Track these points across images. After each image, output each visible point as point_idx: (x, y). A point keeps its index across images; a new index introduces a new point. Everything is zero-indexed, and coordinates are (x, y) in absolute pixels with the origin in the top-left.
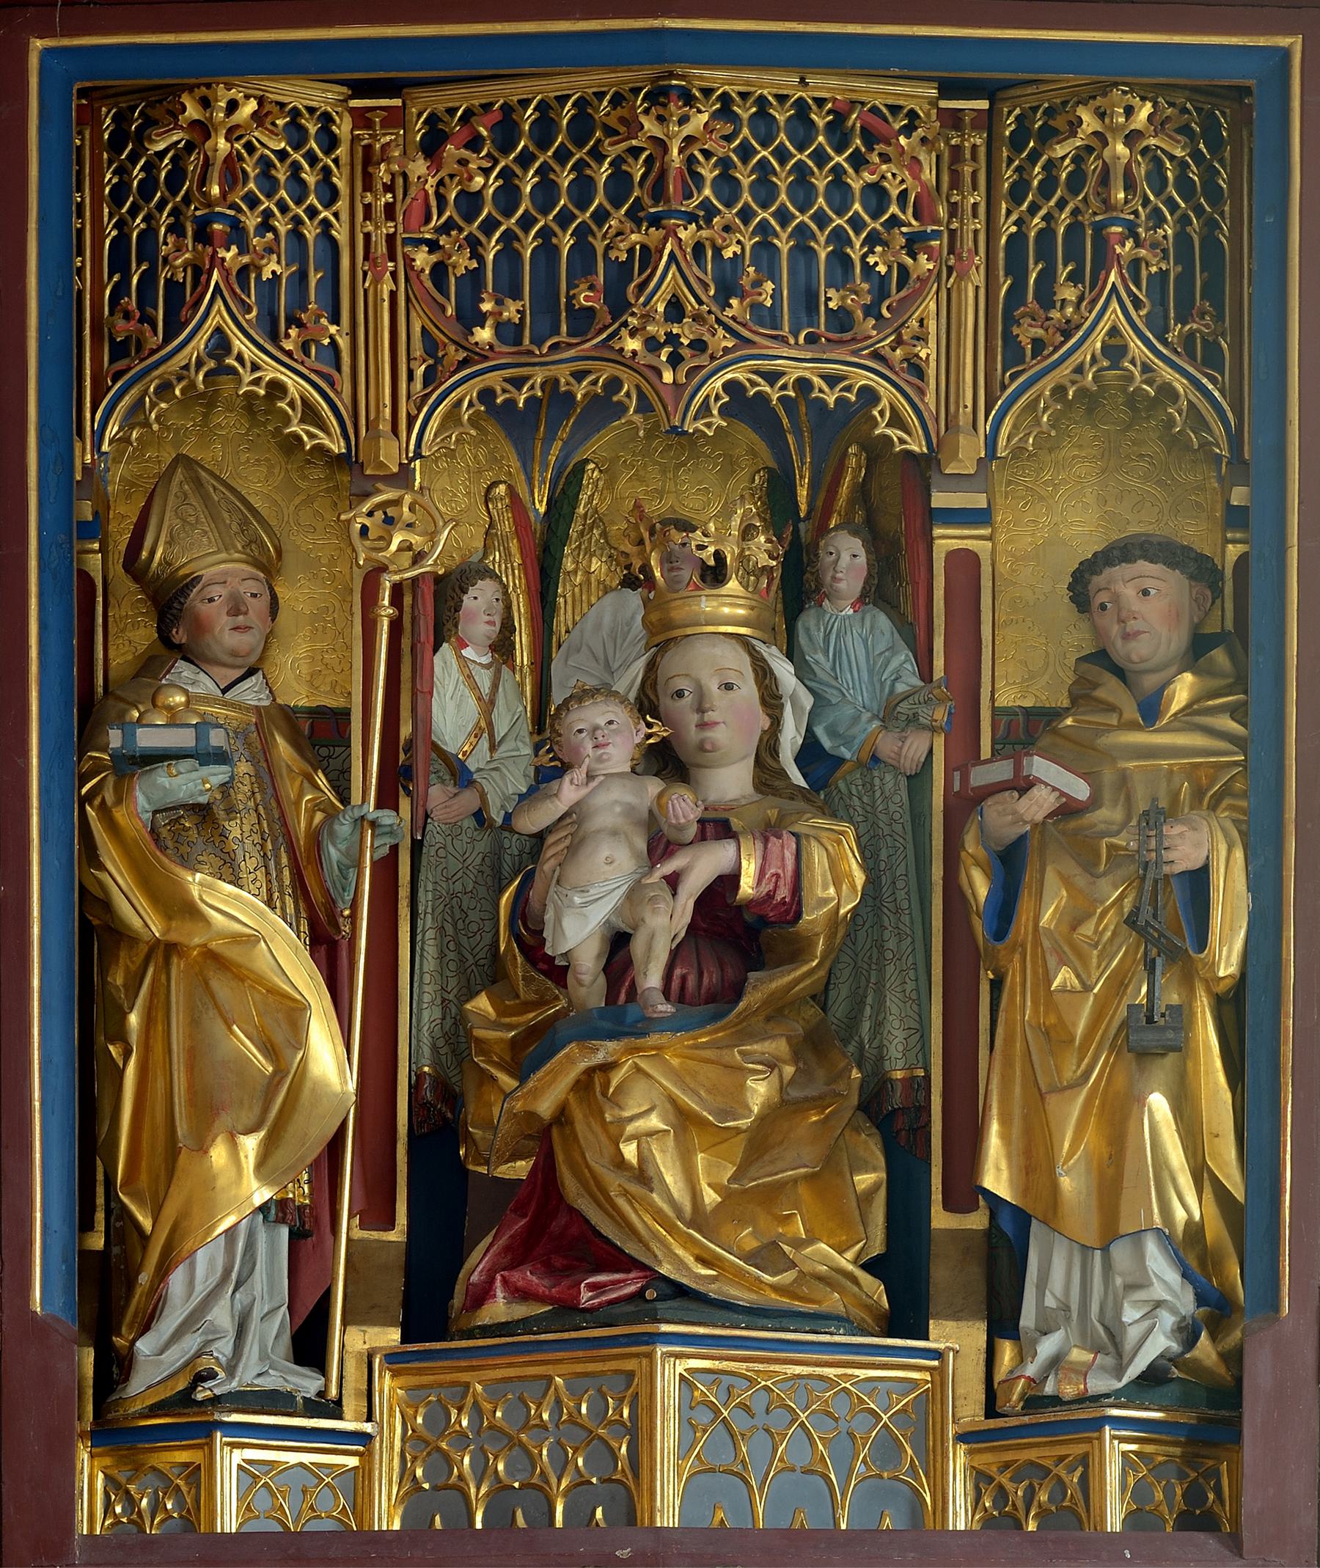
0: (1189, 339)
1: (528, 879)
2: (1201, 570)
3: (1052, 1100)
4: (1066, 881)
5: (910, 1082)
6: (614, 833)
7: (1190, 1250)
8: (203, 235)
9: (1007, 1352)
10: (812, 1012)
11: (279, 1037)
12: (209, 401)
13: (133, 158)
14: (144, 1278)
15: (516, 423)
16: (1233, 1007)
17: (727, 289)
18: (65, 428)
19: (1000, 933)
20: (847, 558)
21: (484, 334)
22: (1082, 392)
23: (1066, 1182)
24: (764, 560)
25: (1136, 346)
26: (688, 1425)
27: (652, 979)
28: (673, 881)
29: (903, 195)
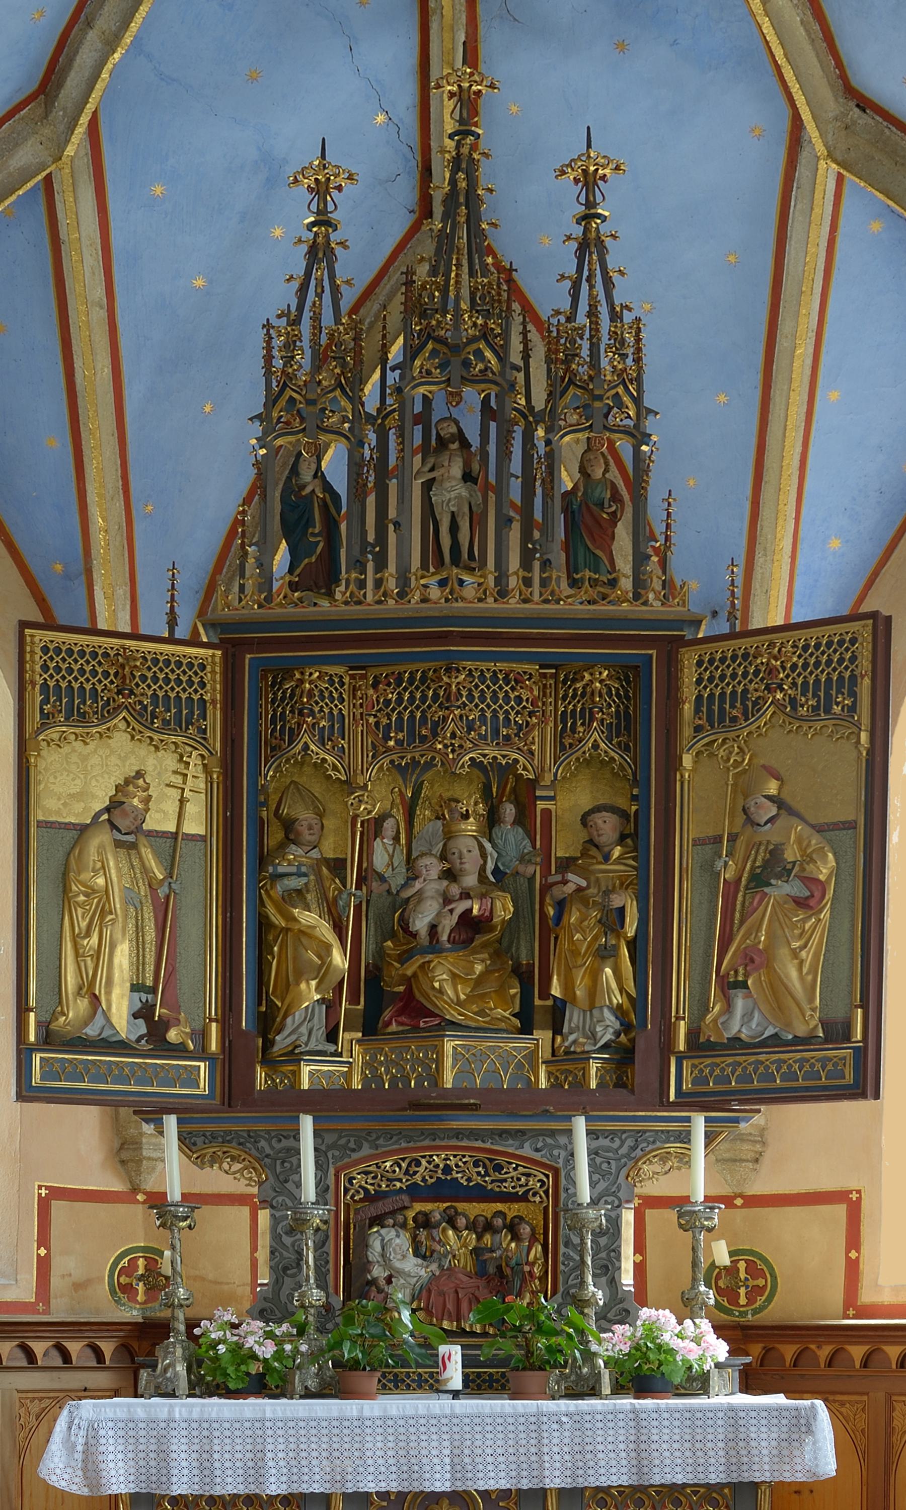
0: (619, 743)
1: (404, 910)
2: (623, 814)
3: (574, 970)
4: (579, 910)
5: (528, 964)
6: (432, 898)
7: (618, 1011)
8: (301, 713)
9: (559, 1039)
10: (496, 945)
11: (323, 954)
12: (302, 763)
13: (278, 690)
14: (278, 1019)
15: (403, 771)
16: (632, 945)
17: (470, 729)
18: (255, 773)
19: (557, 925)
20: (509, 811)
21: (392, 743)
22: (585, 759)
23: (578, 993)
24: (481, 812)
25: (602, 745)
26: (455, 1060)
27: (445, 938)
28: (451, 911)
29: (527, 700)
